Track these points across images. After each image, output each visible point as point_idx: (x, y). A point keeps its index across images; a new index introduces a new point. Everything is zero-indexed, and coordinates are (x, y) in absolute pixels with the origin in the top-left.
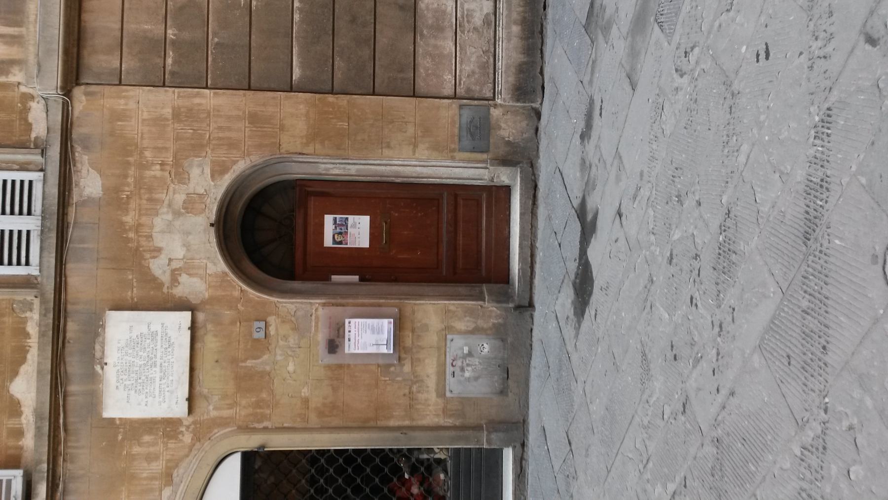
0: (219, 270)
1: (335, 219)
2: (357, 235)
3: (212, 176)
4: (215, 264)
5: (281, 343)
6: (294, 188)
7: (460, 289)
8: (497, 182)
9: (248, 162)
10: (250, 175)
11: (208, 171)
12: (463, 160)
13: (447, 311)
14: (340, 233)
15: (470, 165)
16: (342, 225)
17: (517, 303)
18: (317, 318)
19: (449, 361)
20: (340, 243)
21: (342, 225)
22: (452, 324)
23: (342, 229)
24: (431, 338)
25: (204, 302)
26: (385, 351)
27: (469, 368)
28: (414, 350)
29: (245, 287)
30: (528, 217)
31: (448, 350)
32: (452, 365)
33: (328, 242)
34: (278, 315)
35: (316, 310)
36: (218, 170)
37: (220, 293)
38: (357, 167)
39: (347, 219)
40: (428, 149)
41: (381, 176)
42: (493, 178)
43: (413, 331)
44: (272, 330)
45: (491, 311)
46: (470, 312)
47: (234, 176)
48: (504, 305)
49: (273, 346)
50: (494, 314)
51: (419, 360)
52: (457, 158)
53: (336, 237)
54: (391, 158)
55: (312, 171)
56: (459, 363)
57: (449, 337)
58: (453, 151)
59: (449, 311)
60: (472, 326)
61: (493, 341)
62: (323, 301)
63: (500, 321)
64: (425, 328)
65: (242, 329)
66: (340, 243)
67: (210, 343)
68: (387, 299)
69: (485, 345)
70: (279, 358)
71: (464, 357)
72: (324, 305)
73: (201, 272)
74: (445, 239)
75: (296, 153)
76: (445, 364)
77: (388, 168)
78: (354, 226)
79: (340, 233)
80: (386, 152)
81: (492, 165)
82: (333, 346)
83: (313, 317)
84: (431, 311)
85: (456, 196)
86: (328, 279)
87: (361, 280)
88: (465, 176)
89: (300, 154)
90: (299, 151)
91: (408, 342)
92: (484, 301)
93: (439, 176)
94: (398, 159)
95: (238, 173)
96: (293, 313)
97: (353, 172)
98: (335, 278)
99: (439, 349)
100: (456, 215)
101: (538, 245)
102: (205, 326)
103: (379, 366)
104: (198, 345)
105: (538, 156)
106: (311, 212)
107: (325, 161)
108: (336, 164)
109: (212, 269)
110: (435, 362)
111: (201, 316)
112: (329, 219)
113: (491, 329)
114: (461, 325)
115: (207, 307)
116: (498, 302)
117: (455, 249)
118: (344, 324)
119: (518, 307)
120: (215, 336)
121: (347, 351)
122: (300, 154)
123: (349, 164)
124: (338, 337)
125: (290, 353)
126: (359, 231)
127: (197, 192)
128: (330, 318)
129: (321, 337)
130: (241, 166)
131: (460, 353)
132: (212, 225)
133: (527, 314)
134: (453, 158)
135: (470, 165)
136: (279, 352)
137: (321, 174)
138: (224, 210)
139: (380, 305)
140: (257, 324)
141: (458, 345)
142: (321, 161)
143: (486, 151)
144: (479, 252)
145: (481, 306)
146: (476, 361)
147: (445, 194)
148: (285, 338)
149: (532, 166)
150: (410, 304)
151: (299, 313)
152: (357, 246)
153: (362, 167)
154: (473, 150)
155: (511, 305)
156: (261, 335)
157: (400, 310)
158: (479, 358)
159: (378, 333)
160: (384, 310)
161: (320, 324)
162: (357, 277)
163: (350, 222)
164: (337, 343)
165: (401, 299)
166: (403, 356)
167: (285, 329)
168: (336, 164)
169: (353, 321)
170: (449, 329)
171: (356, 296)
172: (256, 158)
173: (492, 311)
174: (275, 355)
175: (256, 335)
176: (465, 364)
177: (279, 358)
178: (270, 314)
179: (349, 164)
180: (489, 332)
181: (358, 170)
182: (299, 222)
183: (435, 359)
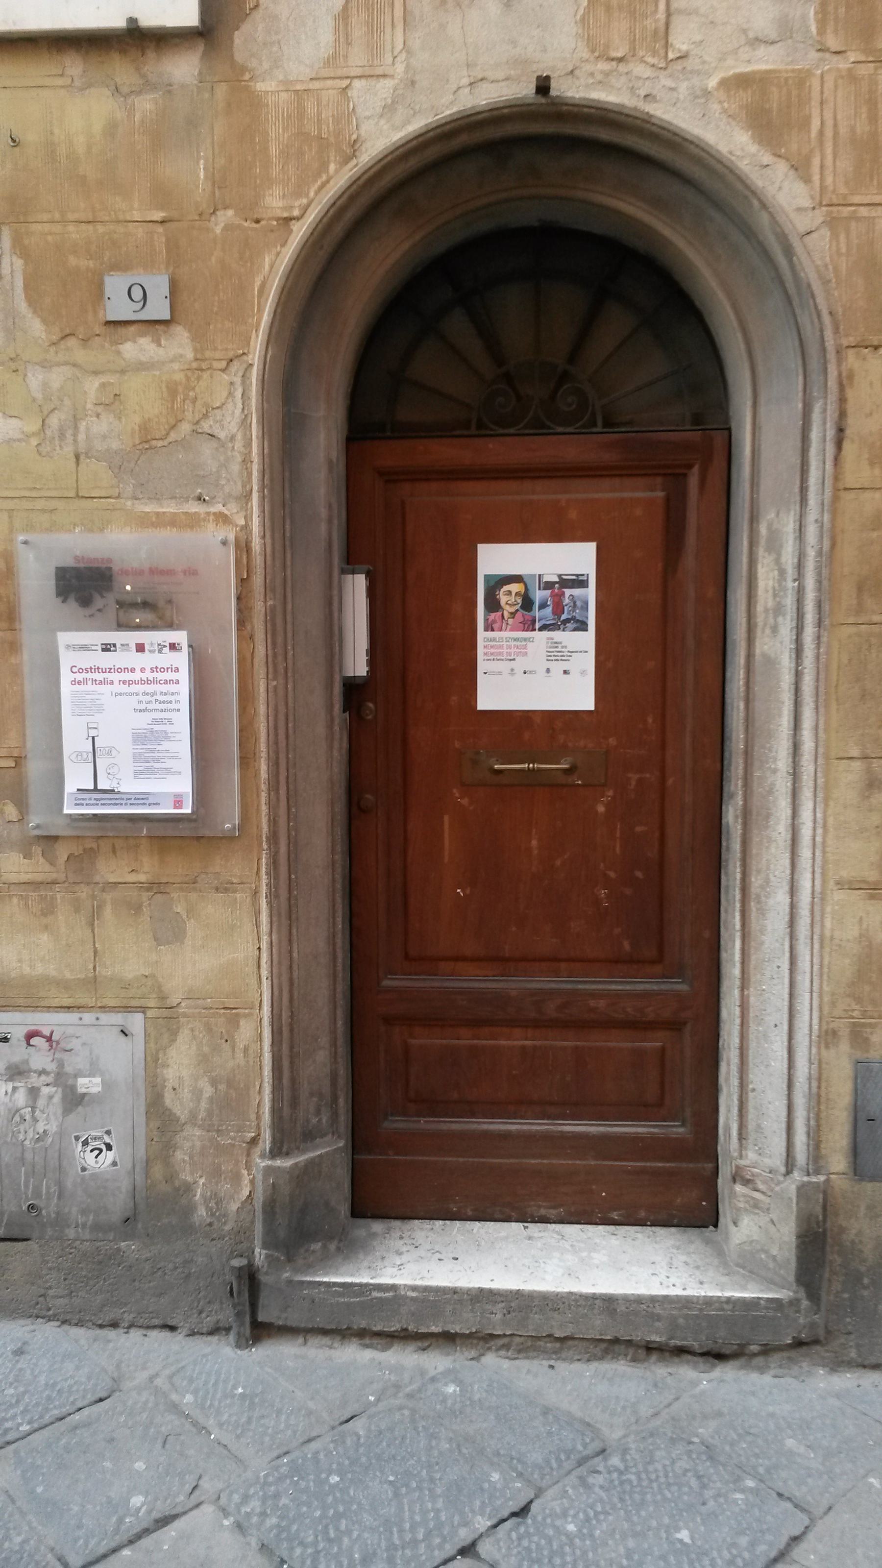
0: (366, 128)
1: (580, 582)
2: (520, 664)
3: (742, 81)
4: (389, 109)
5: (92, 385)
6: (697, 420)
7: (322, 1056)
8: (733, 1196)
9: (802, 223)
10: (749, 232)
11: (764, 61)
12: (819, 1078)
13: (233, 1015)
14: (527, 603)
15: (800, 1101)
16: (558, 609)
17: (263, 1278)
18: (193, 522)
19: (45, 1021)
20: (493, 605)
21: (558, 609)
22: (184, 1036)
23: (541, 608)
24: (129, 954)
25: (238, 79)
26: (70, 787)
27: (21, 1098)
28: (83, 892)
29: (300, 232)
30: (598, 1326)
31: (88, 1017)
32: (30, 1036)
33: (495, 559)
34: (200, 366)
35: (223, 519)
36: (768, 105)
37: (277, 135)
38: (786, 661)
39: (582, 626)
40: (864, 937)
41: (392, 152)
42: (747, 1182)
43: (156, 887)
44: (138, 348)
45: (236, 1178)
46: (230, 1100)
47: (744, 166)
48: (259, 1229)
49: (80, 355)
50: (226, 1187)
51: (49, 910)
52: (829, 1055)
53: (515, 588)
54: (825, 793)
55: (767, 484)
56: (40, 1058)
57: (136, 1023)
58: (859, 1036)
59: (234, 1021)
60: (179, 1105)
61: (125, 1185)
62: (256, 544)
63: (202, 1211)
64: (170, 933)
65: (140, 232)
66: (493, 605)
67: (80, 111)
68: (274, 787)
69: (109, 1157)
70: (35, 379)
71: (63, 1080)
72: (243, 547)
73: (357, 58)
74: (516, 985)
75: (842, 414)
76: (35, 1008)
77: (782, 784)
78: (556, 654)
79: (527, 603)
80: (850, 775)
81: (802, 1189)
82: (86, 587)
83: (194, 508)
84: (230, 958)
85: (675, 1026)
86: (352, 560)
87: (354, 691)
88: (755, 1077)
89: (841, 430)
90: (853, 425)
91: (112, 870)
92: (277, 1151)
93: (754, 978)
94: (822, 825)
95: (757, 179)
96: (206, 426)
97: (764, 645)
98: (357, 586)
99: (93, 982)
100: (608, 1024)
101: (490, 1359)
102: (148, 86)
103: (19, 760)
104: (74, 65)
105: (838, 1364)
106: (605, 492)
107: (812, 531)
108: (800, 576)
109: (368, 97)
110: (40, 969)
111: (183, 68)
112: (579, 558)
113: (170, 1178)
114: (181, 1064)
115: (222, 91)
116: (270, 1208)
117: (477, 1023)
118: (170, 626)
119: (250, 1279)
120: (111, 129)
121: (64, 638)
122: (841, 430)
123: (799, 629)
124: (121, 604)
125: (54, 421)
126: (537, 672)
127: (677, 22)
128: (191, 572)
129: (120, 542)
130: (786, 194)
131: (76, 1062)
132: (543, 87)
133: (226, 1314)
134: (827, 1037)
135: (800, 1101)
136: (57, 378)
137: (754, 519)
138: (604, 135)
139: (246, 760)
140: (158, 286)
141: (107, 1054)
142: (812, 514)
143: (859, 1168)
144: (471, 1109)
145: (254, 1141)
146: (49, 1120)
147: (684, 988)
148: (112, 402)
149: (799, 1344)
150: (251, 873)
151: (207, 449)
152: (482, 665)
153: (787, 679)
154: (862, 1119)
155: (260, 1255)
156: (119, 307)
157: (229, 838)
158: (61, 1134)
159: (137, 758)
160: (232, 777)
161: (167, 534)
162: (358, 665)
163: (568, 638)
164: (99, 602)
165: (273, 838)
166: (62, 852)
167: (144, 400)
168: (800, 576)
169: (182, 660)
170: (166, 1020)
171: (281, 665)
172: (818, 251)
173: (237, 1180)
174: (46, 365)
175: (115, 285)
176: (35, 1080)
177: (35, 379)
178: (199, 337)
179: (799, 629)
180: (158, 1171)
181: (771, 662)
182: (569, 448)
183: (52, 970)
